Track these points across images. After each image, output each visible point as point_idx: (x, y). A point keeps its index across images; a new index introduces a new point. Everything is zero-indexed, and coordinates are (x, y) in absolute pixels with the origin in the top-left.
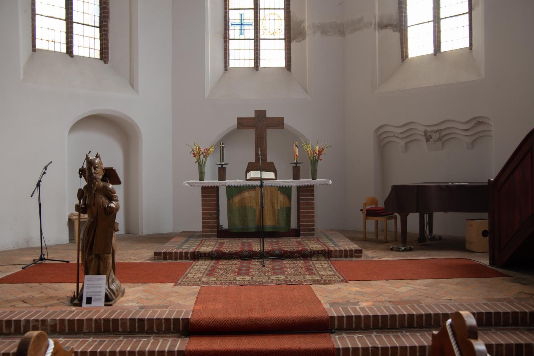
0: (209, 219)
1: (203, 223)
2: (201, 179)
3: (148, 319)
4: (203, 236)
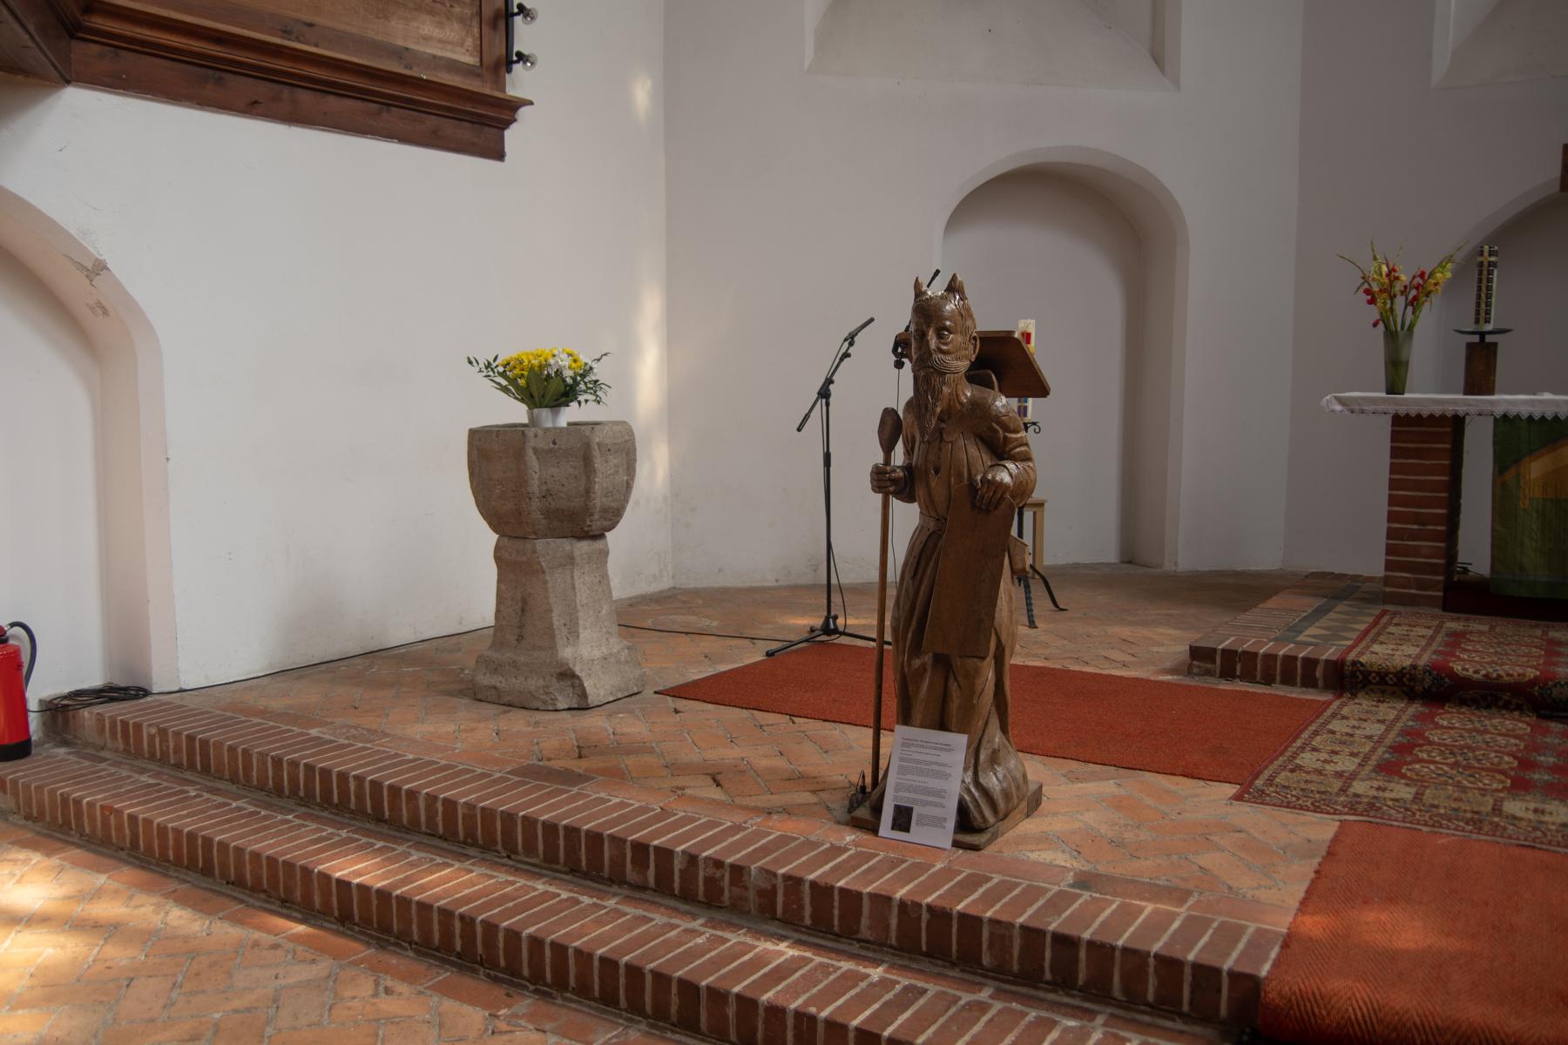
0: (1413, 536)
1: (1390, 550)
3: (1091, 944)
4: (1387, 599)
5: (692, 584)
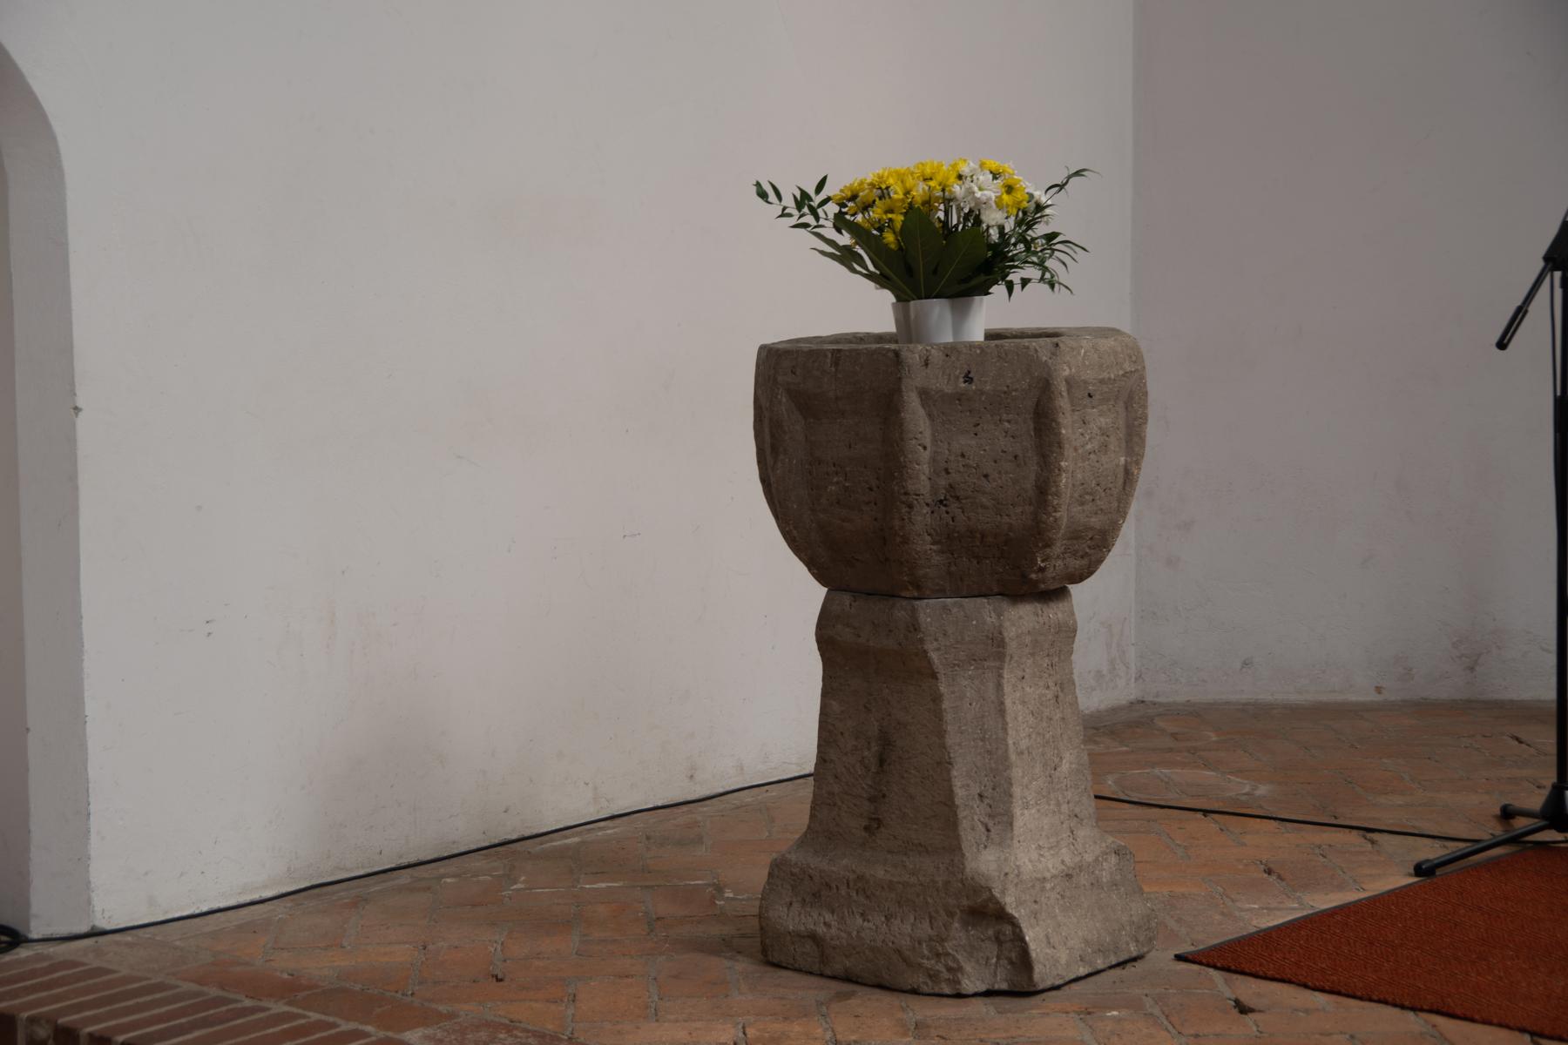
5: (1180, 693)
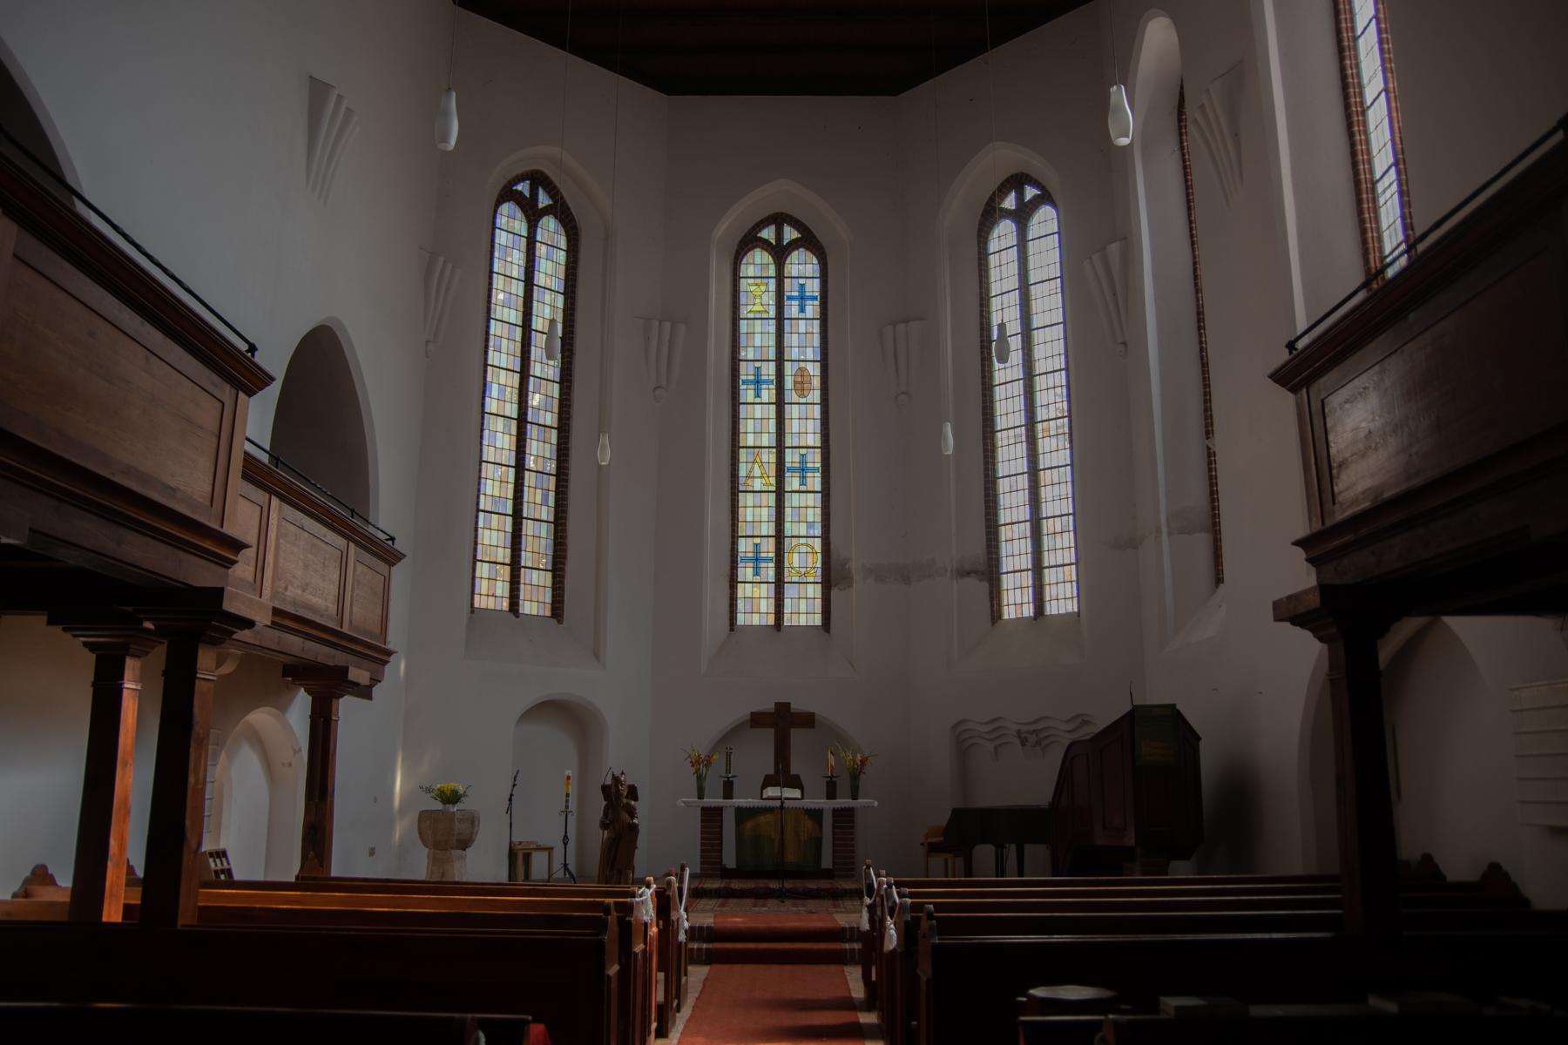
2: (701, 797)
